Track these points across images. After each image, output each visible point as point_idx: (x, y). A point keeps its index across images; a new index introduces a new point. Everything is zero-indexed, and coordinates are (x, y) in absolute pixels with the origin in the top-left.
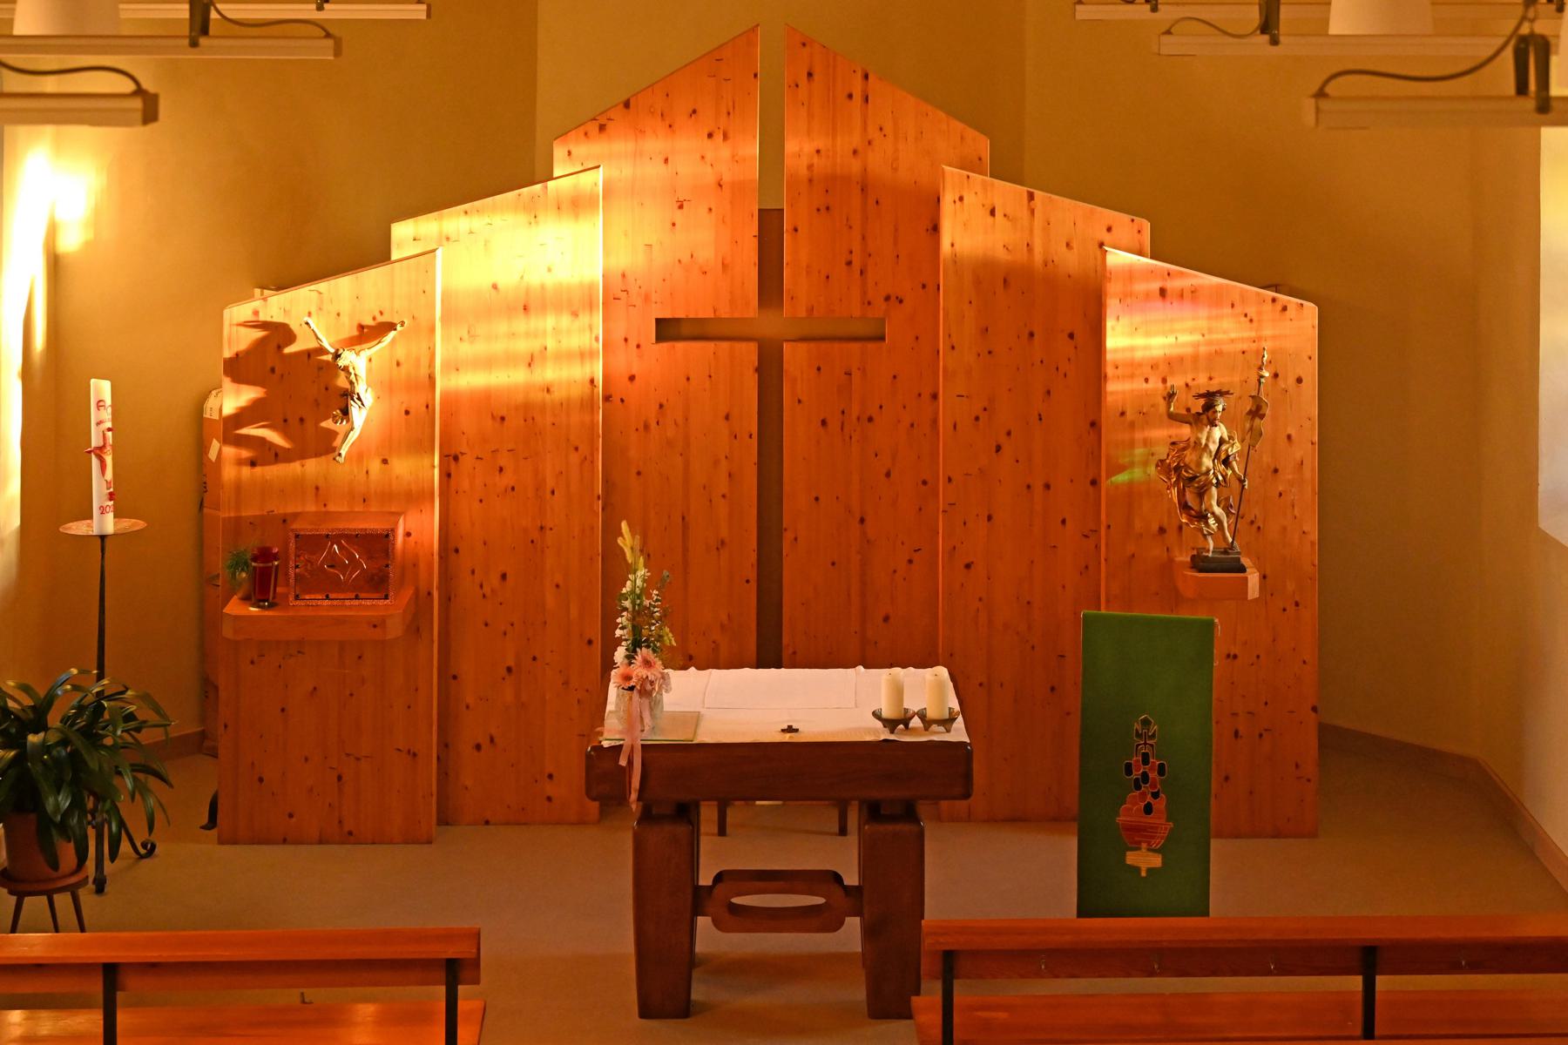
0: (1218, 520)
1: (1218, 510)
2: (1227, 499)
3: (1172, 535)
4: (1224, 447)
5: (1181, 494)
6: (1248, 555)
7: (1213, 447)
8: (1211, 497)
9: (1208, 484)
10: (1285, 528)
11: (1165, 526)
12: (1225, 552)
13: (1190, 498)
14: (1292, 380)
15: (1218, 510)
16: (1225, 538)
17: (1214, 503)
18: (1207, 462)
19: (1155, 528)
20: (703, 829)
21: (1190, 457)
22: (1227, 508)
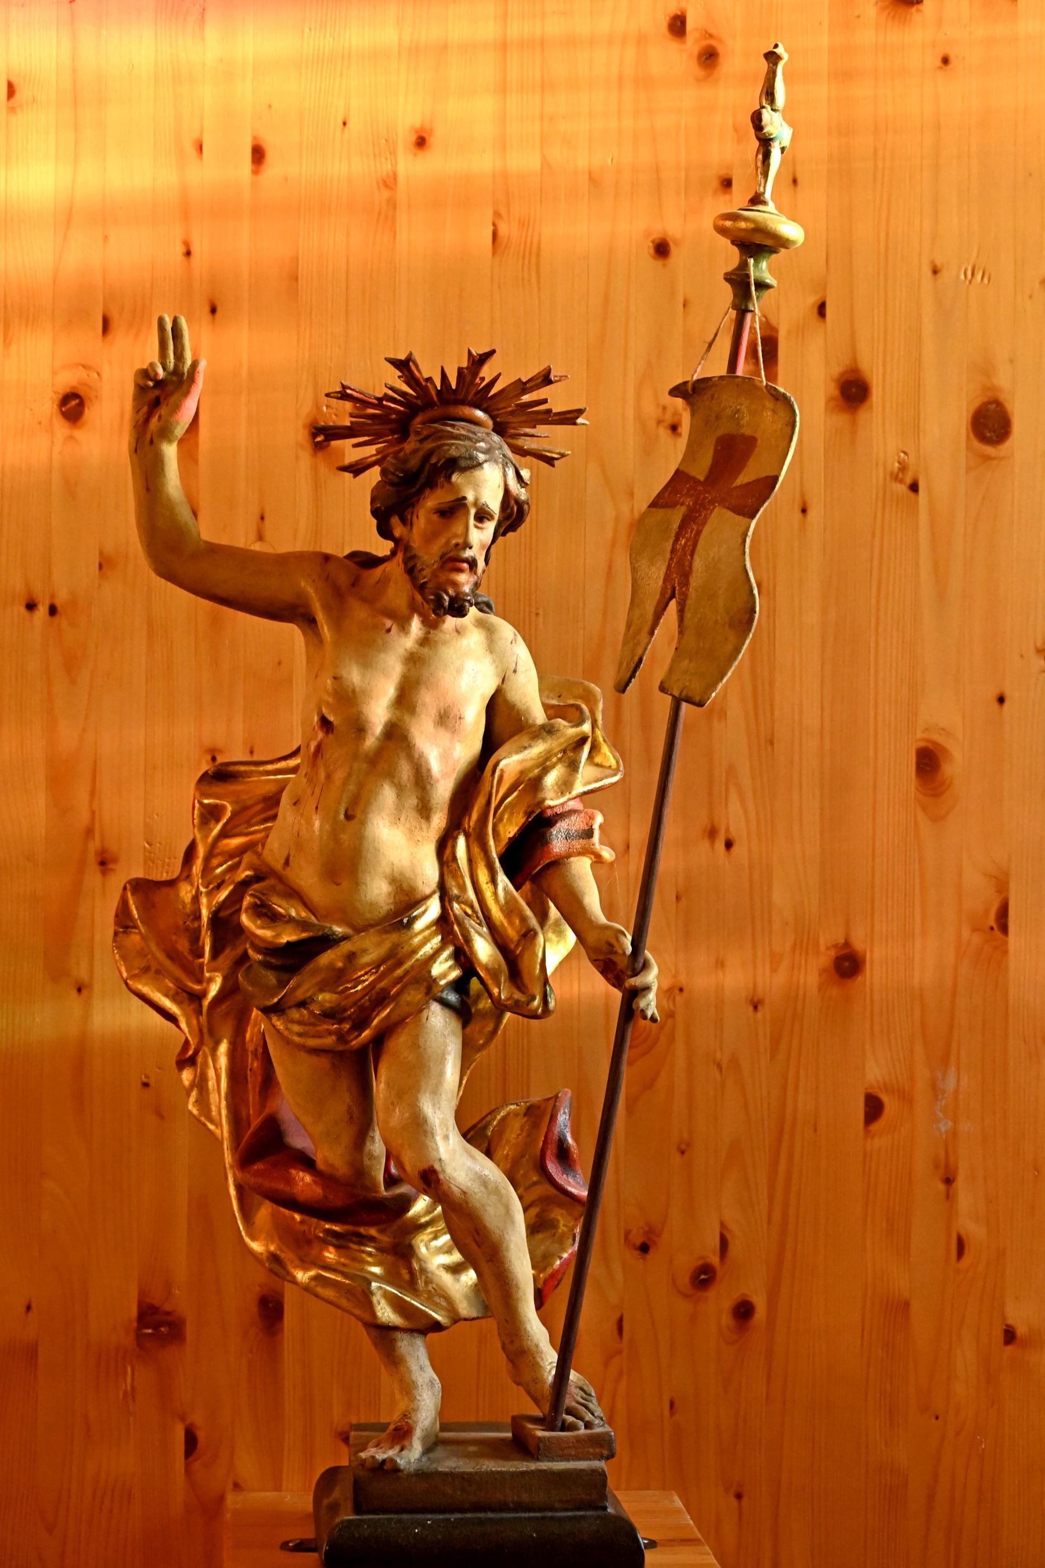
0: (477, 1245)
1: (460, 1163)
2: (539, 1114)
3: (214, 1359)
4: (511, 762)
5: (253, 1078)
6: (679, 1476)
7: (445, 755)
8: (418, 1072)
9: (401, 986)
10: (899, 1309)
11: (181, 1302)
12: (521, 1445)
13: (310, 1125)
14: (947, 422)
15: (460, 1163)
16: (518, 1353)
17: (439, 1112)
18: (401, 846)
19: (113, 1307)
20: (373, 1421)
21: (297, 832)
22: (535, 1164)
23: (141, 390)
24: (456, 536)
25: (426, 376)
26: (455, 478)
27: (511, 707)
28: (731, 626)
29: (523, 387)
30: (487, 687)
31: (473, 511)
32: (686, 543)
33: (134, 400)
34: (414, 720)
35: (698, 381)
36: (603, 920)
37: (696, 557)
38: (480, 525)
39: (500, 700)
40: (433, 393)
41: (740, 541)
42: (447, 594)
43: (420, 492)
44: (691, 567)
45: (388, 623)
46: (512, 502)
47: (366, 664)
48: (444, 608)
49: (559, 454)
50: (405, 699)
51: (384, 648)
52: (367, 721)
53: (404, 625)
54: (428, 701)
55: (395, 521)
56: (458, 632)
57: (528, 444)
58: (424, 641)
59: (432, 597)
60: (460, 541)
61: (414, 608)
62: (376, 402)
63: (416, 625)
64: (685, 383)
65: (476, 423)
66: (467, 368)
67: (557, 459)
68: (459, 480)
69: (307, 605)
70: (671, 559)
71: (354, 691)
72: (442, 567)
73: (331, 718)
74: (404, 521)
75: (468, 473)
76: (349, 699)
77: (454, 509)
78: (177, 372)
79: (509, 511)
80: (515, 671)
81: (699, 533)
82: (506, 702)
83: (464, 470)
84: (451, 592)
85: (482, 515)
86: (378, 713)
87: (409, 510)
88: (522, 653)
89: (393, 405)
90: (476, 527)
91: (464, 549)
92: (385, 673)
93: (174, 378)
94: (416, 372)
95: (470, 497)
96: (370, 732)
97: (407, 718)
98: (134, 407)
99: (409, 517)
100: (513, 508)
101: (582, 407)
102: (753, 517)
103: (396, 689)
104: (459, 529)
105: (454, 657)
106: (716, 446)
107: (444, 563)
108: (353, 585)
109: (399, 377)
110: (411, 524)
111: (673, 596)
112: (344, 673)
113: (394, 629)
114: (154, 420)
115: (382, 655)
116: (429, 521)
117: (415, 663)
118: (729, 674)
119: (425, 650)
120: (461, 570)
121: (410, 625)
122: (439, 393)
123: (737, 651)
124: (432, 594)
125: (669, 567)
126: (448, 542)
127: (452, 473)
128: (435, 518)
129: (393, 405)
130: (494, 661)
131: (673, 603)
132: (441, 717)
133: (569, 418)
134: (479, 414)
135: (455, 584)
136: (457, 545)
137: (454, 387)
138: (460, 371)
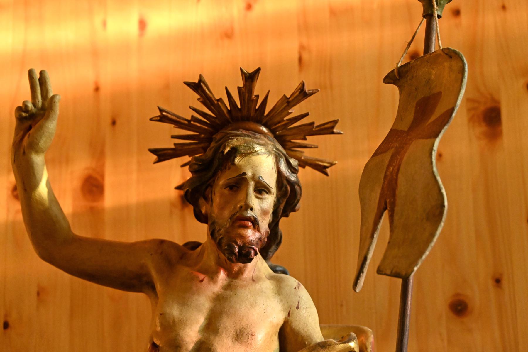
23: (20, 119)
24: (240, 201)
25: (217, 98)
26: (237, 160)
27: (296, 334)
28: (428, 219)
29: (288, 102)
30: (277, 317)
31: (252, 185)
32: (393, 169)
33: (16, 130)
34: (217, 338)
35: (401, 67)
36: (27, 115)
37: (400, 175)
38: (260, 196)
39: (288, 330)
40: (225, 111)
41: (428, 155)
42: (237, 244)
43: (215, 174)
44: (396, 183)
45: (202, 276)
46: (285, 182)
47: (184, 303)
48: (235, 254)
49: (328, 163)
50: (212, 326)
51: (198, 292)
52: (182, 340)
53: (212, 276)
54: (228, 325)
55: (202, 201)
56: (253, 280)
57: (307, 154)
58: (228, 287)
59: (226, 247)
60: (242, 204)
61: (220, 265)
62: (186, 122)
63: (222, 275)
64: (393, 71)
65: (261, 133)
66: (243, 87)
67: (328, 167)
68: (241, 163)
69: (148, 275)
70: (384, 182)
71: (174, 322)
72: (232, 225)
73: (157, 342)
74: (206, 199)
75: (247, 158)
76: (170, 329)
77: (239, 183)
78: (43, 108)
79: (284, 189)
80: (298, 307)
81: (401, 160)
82: (292, 329)
83: (244, 155)
84: (240, 242)
85: (261, 189)
86: (191, 335)
87: (209, 189)
88: (304, 295)
89: (199, 125)
90: (257, 197)
91: (246, 210)
92: (198, 309)
93: (42, 112)
94: (207, 91)
95: (249, 174)
96: (184, 348)
97: (212, 337)
98: (15, 134)
99: (210, 196)
100: (286, 187)
101: (336, 119)
102: (436, 136)
103: (206, 319)
104: (241, 196)
105: (249, 296)
106: (416, 107)
107: (234, 222)
108: (181, 258)
109: (198, 99)
110: (212, 201)
111: (385, 209)
112: (168, 310)
113: (206, 280)
114: (26, 138)
115: (196, 297)
116: (222, 195)
117: (220, 300)
118: (427, 253)
119: (228, 292)
120: (247, 227)
121: (217, 276)
122: (229, 112)
123: (433, 235)
124: (225, 246)
125: (383, 188)
126: (235, 208)
127: (235, 157)
128: (226, 191)
129: (199, 125)
130: (282, 301)
131: (386, 214)
132: (237, 335)
133: (328, 129)
134: (264, 129)
135: (242, 237)
136: (241, 207)
137: (239, 107)
138: (239, 89)
